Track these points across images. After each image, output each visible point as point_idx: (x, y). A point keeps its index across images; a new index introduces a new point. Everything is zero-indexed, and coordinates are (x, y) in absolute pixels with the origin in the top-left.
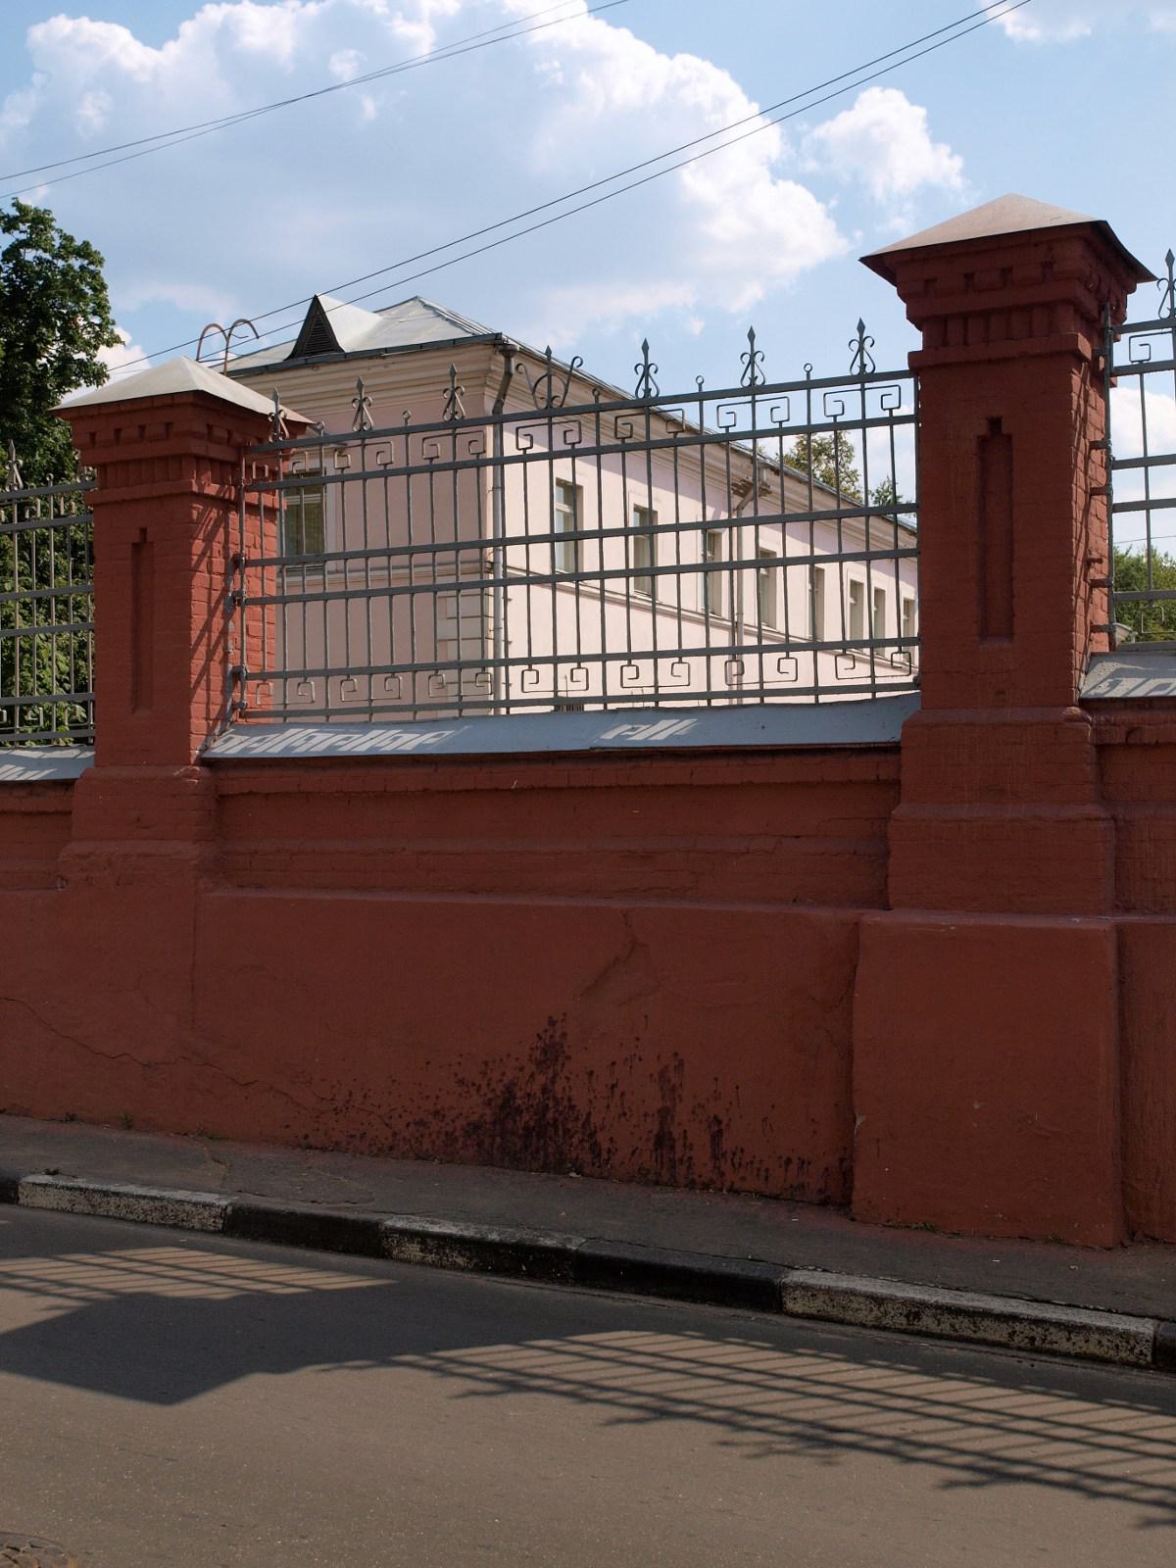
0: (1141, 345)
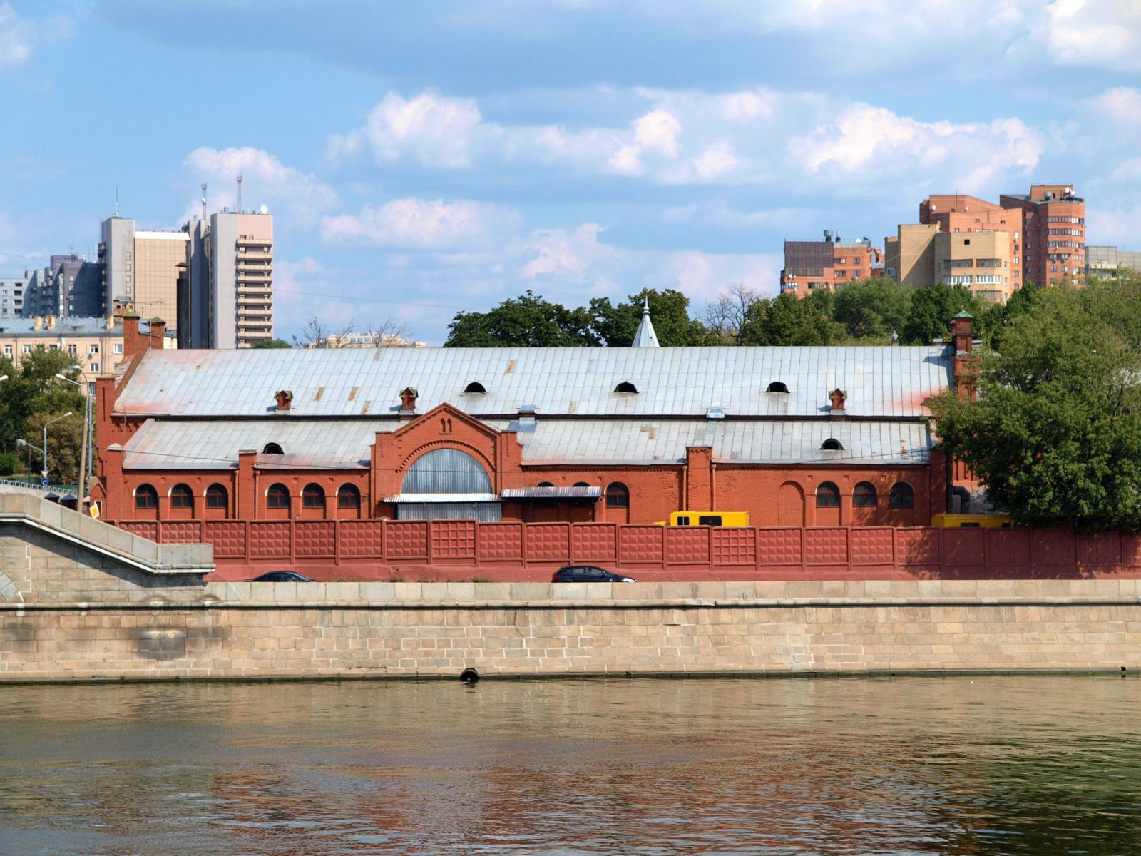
0: (899, 226)
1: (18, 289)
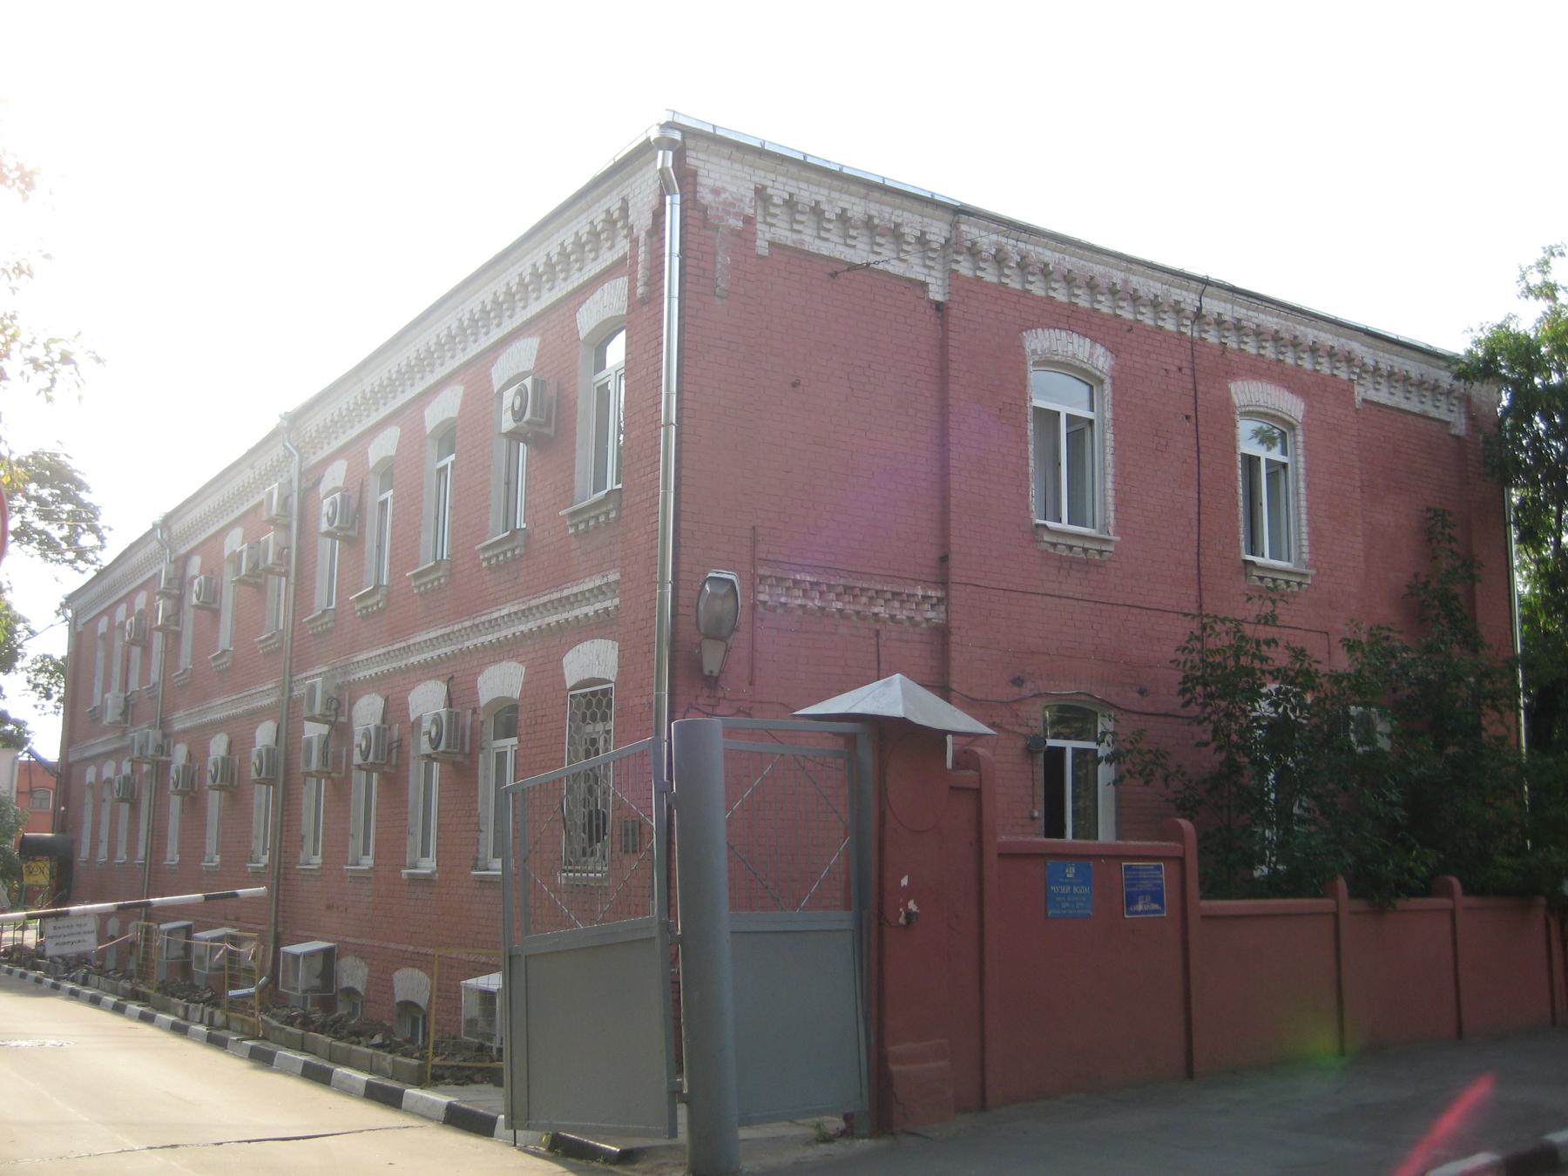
0: (667, 110)
1: (40, 707)
